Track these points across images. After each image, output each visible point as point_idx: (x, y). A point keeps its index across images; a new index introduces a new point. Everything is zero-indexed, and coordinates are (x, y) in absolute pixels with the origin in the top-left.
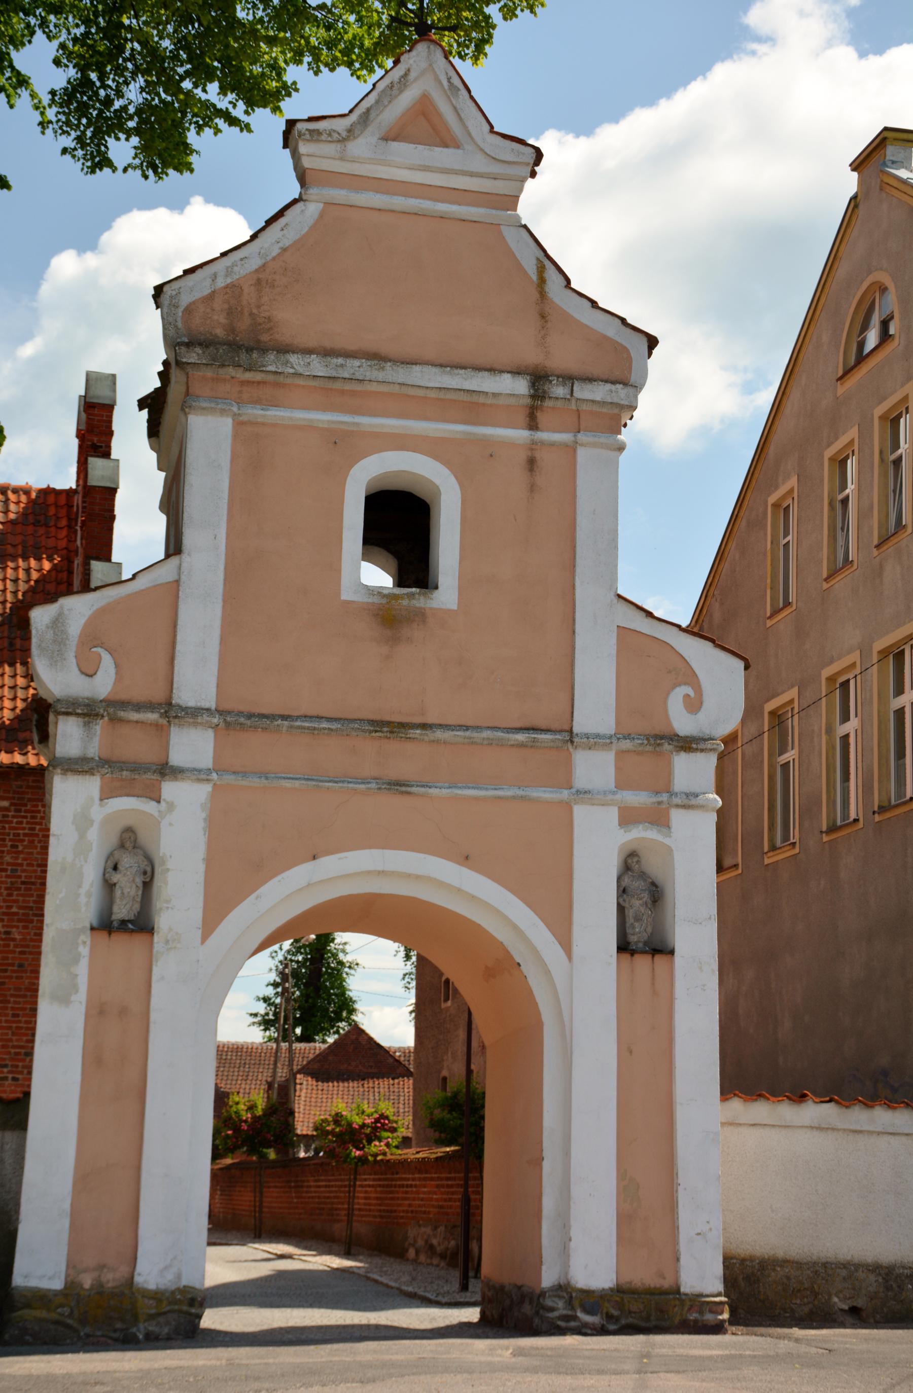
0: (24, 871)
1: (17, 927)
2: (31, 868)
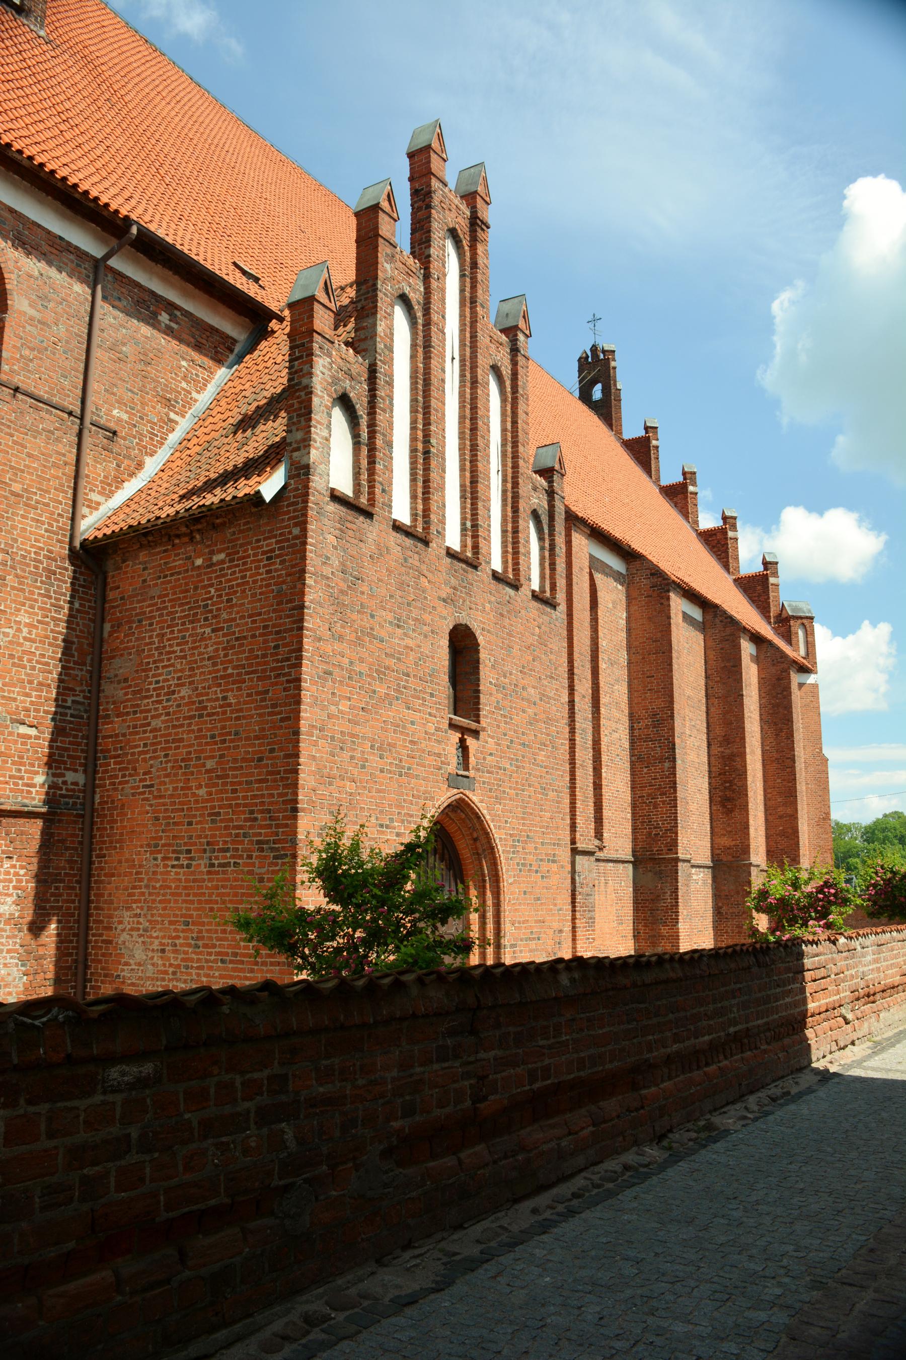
0: (237, 625)
1: (232, 690)
2: (243, 621)
